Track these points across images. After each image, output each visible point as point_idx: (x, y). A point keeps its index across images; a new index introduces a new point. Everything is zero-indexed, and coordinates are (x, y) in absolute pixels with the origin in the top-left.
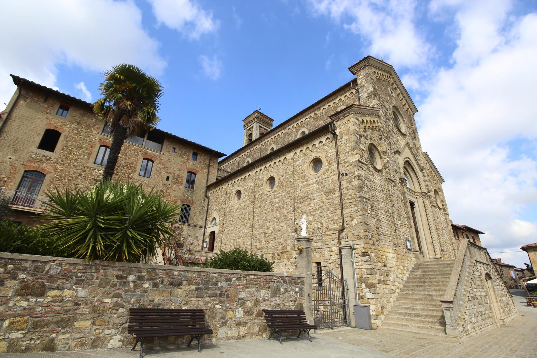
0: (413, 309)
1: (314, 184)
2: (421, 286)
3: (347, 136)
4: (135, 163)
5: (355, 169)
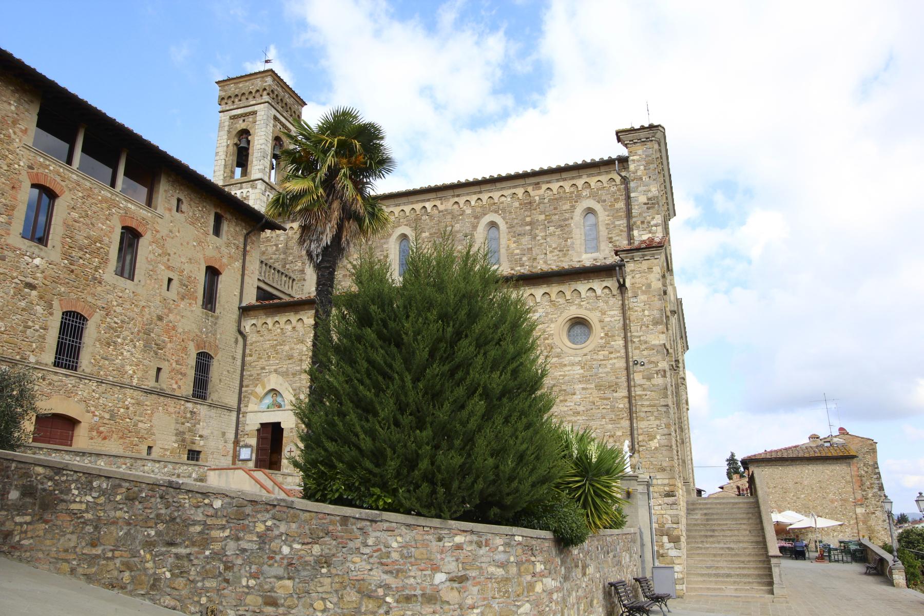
0: (717, 567)
1: (573, 365)
2: (711, 536)
3: (646, 296)
4: (106, 240)
5: (659, 357)
